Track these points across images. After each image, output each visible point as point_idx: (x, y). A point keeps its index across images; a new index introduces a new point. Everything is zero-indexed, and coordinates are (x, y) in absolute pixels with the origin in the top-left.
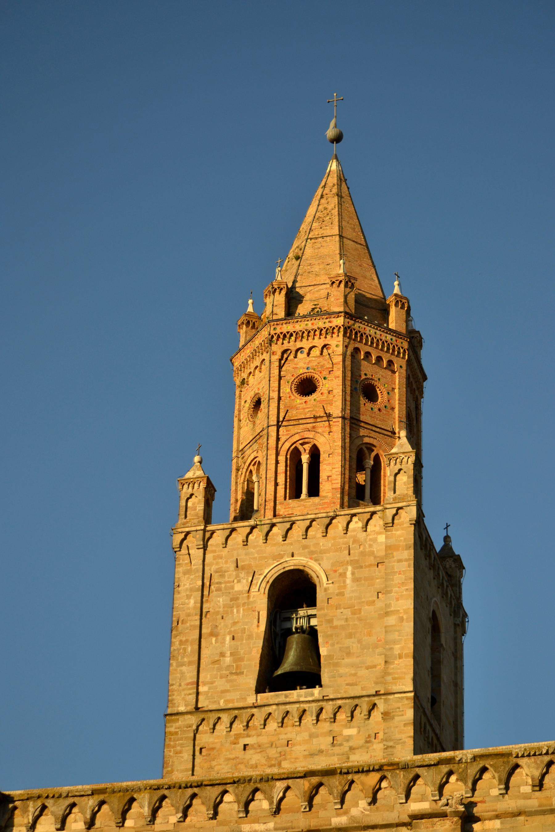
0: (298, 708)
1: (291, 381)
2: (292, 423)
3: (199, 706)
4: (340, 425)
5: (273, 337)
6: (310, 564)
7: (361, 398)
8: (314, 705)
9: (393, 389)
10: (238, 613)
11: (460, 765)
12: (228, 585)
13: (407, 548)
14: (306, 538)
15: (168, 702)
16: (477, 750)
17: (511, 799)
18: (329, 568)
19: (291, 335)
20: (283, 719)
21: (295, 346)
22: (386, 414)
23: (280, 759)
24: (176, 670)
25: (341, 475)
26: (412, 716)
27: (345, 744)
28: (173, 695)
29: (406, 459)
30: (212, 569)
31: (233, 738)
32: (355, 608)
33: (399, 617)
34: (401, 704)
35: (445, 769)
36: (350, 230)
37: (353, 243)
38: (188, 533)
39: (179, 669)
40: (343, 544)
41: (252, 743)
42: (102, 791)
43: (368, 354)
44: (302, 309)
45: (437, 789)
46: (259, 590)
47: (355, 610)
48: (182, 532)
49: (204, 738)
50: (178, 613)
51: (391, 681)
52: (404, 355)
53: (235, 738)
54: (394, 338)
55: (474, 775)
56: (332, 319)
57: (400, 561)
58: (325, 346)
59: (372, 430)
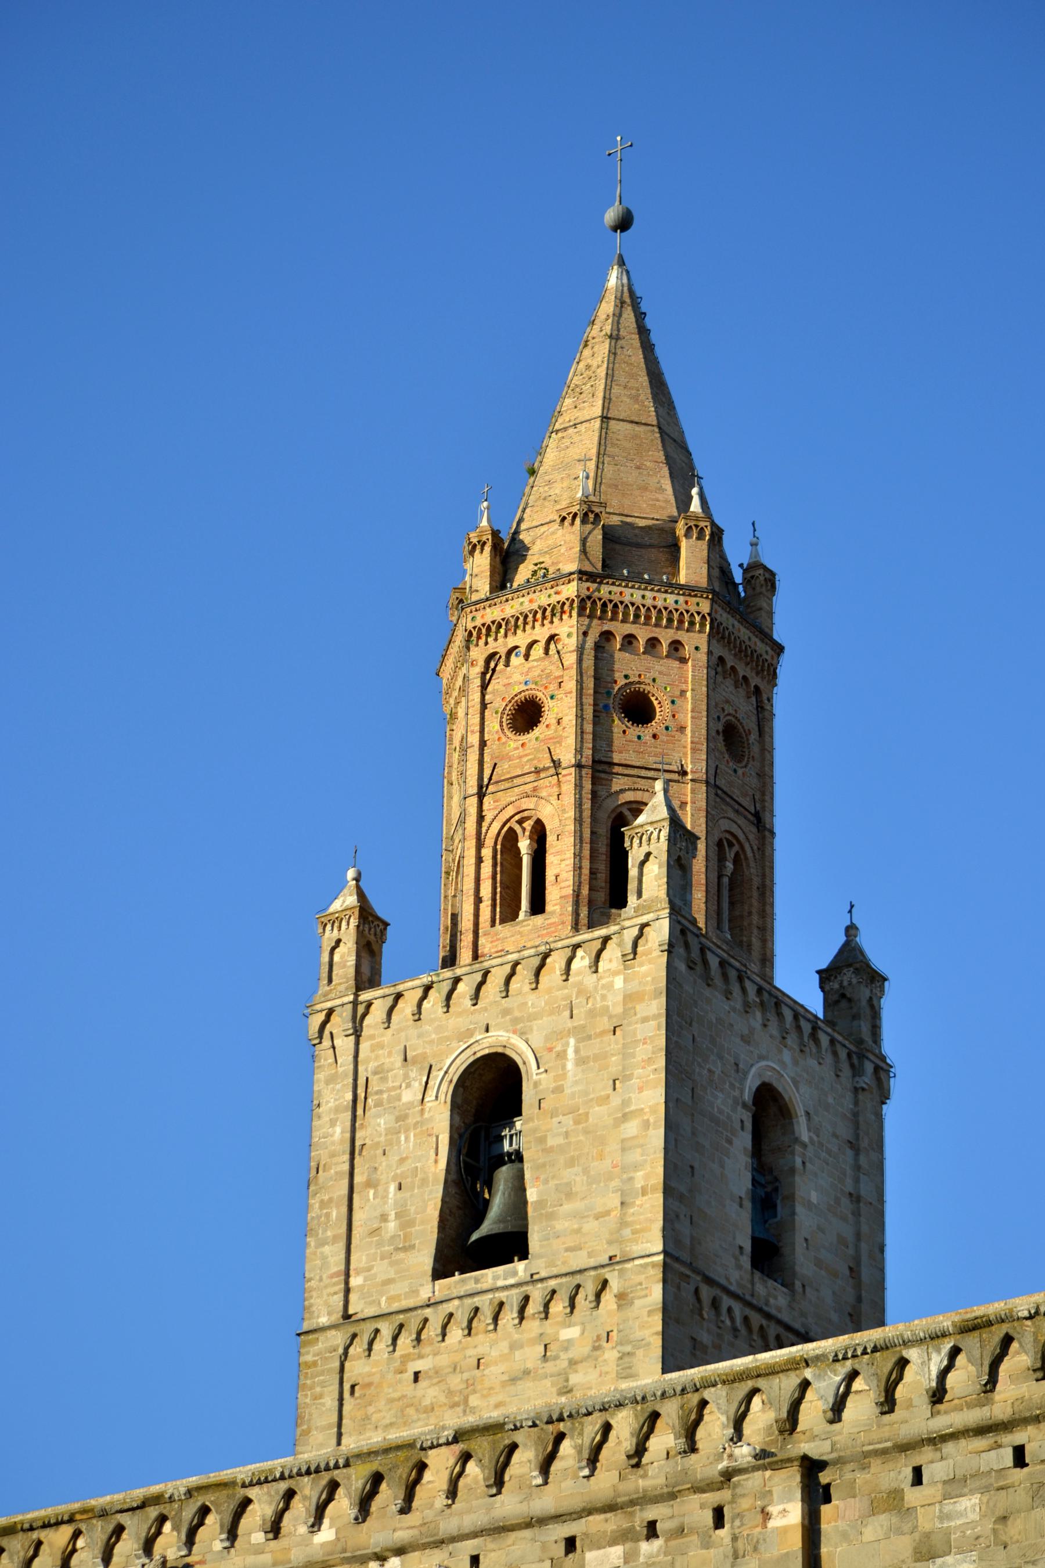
0: (491, 1300)
1: (500, 710)
3: (351, 1312)
4: (573, 780)
5: (470, 634)
6: (513, 1041)
7: (617, 721)
8: (514, 1291)
9: (683, 693)
10: (408, 1142)
11: (173, 1504)
12: (392, 1093)
14: (507, 996)
15: (303, 1309)
16: (194, 1478)
17: (238, 1556)
18: (542, 1045)
19: (500, 626)
20: (470, 1321)
21: (505, 644)
22: (668, 742)
23: (466, 1392)
24: (315, 1253)
25: (574, 870)
26: (661, 1296)
27: (563, 1356)
28: (311, 1297)
29: (655, 834)
30: (369, 1069)
31: (397, 1364)
32: (581, 1111)
33: (643, 1120)
34: (644, 1276)
35: (153, 1512)
36: (628, 400)
37: (629, 426)
38: (330, 1012)
39: (319, 1250)
40: (564, 999)
41: (426, 1368)
43: (629, 640)
44: (523, 573)
45: (141, 1546)
46: (437, 1097)
47: (580, 1115)
48: (321, 1011)
49: (357, 1368)
50: (317, 1153)
51: (631, 1236)
52: (703, 625)
53: (401, 1362)
54: (681, 599)
55: (190, 1520)
56: (559, 588)
57: (645, 1020)
58: (552, 638)
59: (639, 777)
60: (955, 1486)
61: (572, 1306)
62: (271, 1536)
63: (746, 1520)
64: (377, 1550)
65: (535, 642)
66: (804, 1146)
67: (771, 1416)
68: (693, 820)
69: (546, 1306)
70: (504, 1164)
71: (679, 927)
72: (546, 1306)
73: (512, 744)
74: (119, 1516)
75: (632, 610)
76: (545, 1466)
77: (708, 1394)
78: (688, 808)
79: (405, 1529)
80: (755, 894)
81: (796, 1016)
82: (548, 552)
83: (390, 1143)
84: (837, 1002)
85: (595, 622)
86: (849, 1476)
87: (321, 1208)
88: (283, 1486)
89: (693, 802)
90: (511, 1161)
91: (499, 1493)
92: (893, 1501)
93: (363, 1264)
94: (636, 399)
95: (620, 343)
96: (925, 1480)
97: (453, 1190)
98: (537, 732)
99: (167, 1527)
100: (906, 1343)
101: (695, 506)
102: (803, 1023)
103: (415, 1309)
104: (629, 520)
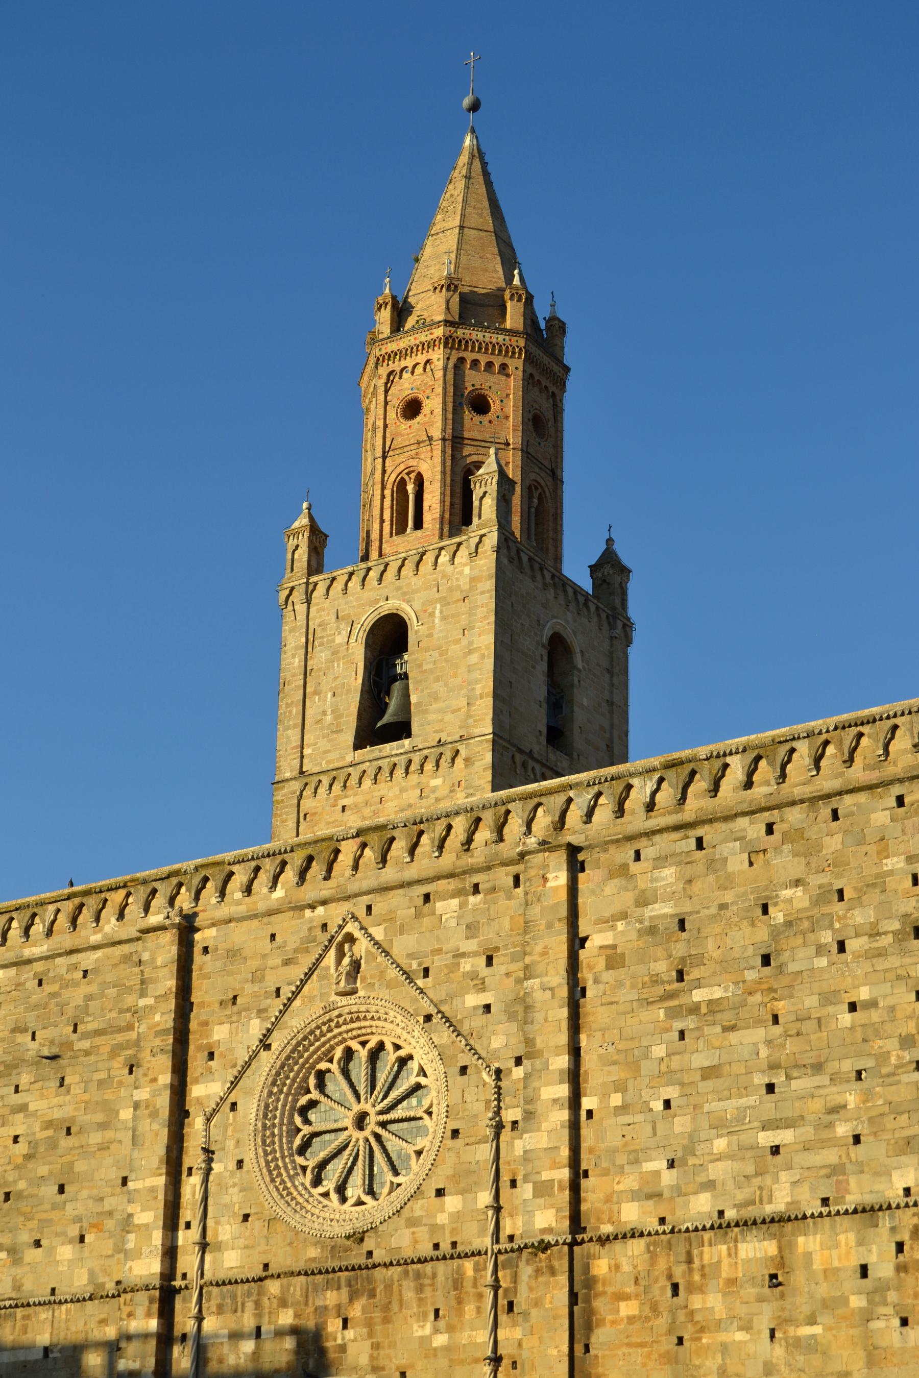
2: (397, 452)
3: (304, 770)
5: (378, 359)
8: (403, 757)
9: (508, 395)
10: (339, 668)
13: (490, 578)
19: (396, 354)
20: (376, 775)
21: (399, 365)
22: (498, 425)
27: (432, 796)
29: (490, 480)
35: (174, 881)
37: (476, 232)
38: (292, 589)
40: (434, 581)
42: (177, 873)
43: (475, 363)
44: (411, 322)
49: (308, 804)
52: (520, 354)
54: (507, 338)
56: (432, 331)
57: (483, 593)
58: (428, 361)
60: (661, 861)
61: (438, 766)
62: (246, 894)
63: (533, 882)
64: (310, 902)
65: (418, 364)
66: (580, 671)
67: (549, 819)
68: (513, 472)
69: (422, 766)
70: (397, 681)
71: (504, 537)
72: (422, 766)
73: (403, 427)
74: (154, 883)
75: (477, 344)
76: (412, 851)
77: (510, 806)
78: (510, 466)
79: (326, 890)
80: (551, 519)
81: (575, 592)
82: (426, 309)
83: (328, 668)
84: (601, 585)
85: (454, 351)
86: (596, 856)
87: (286, 707)
88: (253, 864)
89: (513, 462)
90: (402, 679)
91: (384, 867)
92: (622, 871)
93: (312, 741)
94: (481, 215)
95: (471, 181)
96: (642, 858)
97: (366, 696)
98: (418, 419)
99: (183, 890)
100: (631, 775)
101: (516, 281)
102: (579, 596)
103: (343, 768)
104: (475, 289)
